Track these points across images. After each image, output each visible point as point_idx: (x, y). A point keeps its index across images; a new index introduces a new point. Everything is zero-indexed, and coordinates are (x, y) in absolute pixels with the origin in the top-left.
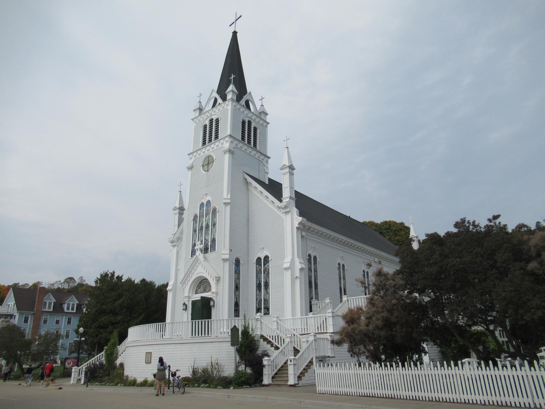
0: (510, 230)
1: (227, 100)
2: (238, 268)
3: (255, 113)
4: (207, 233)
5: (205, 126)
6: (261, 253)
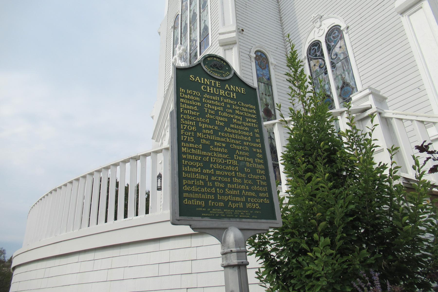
2: (264, 71)
6: (317, 30)
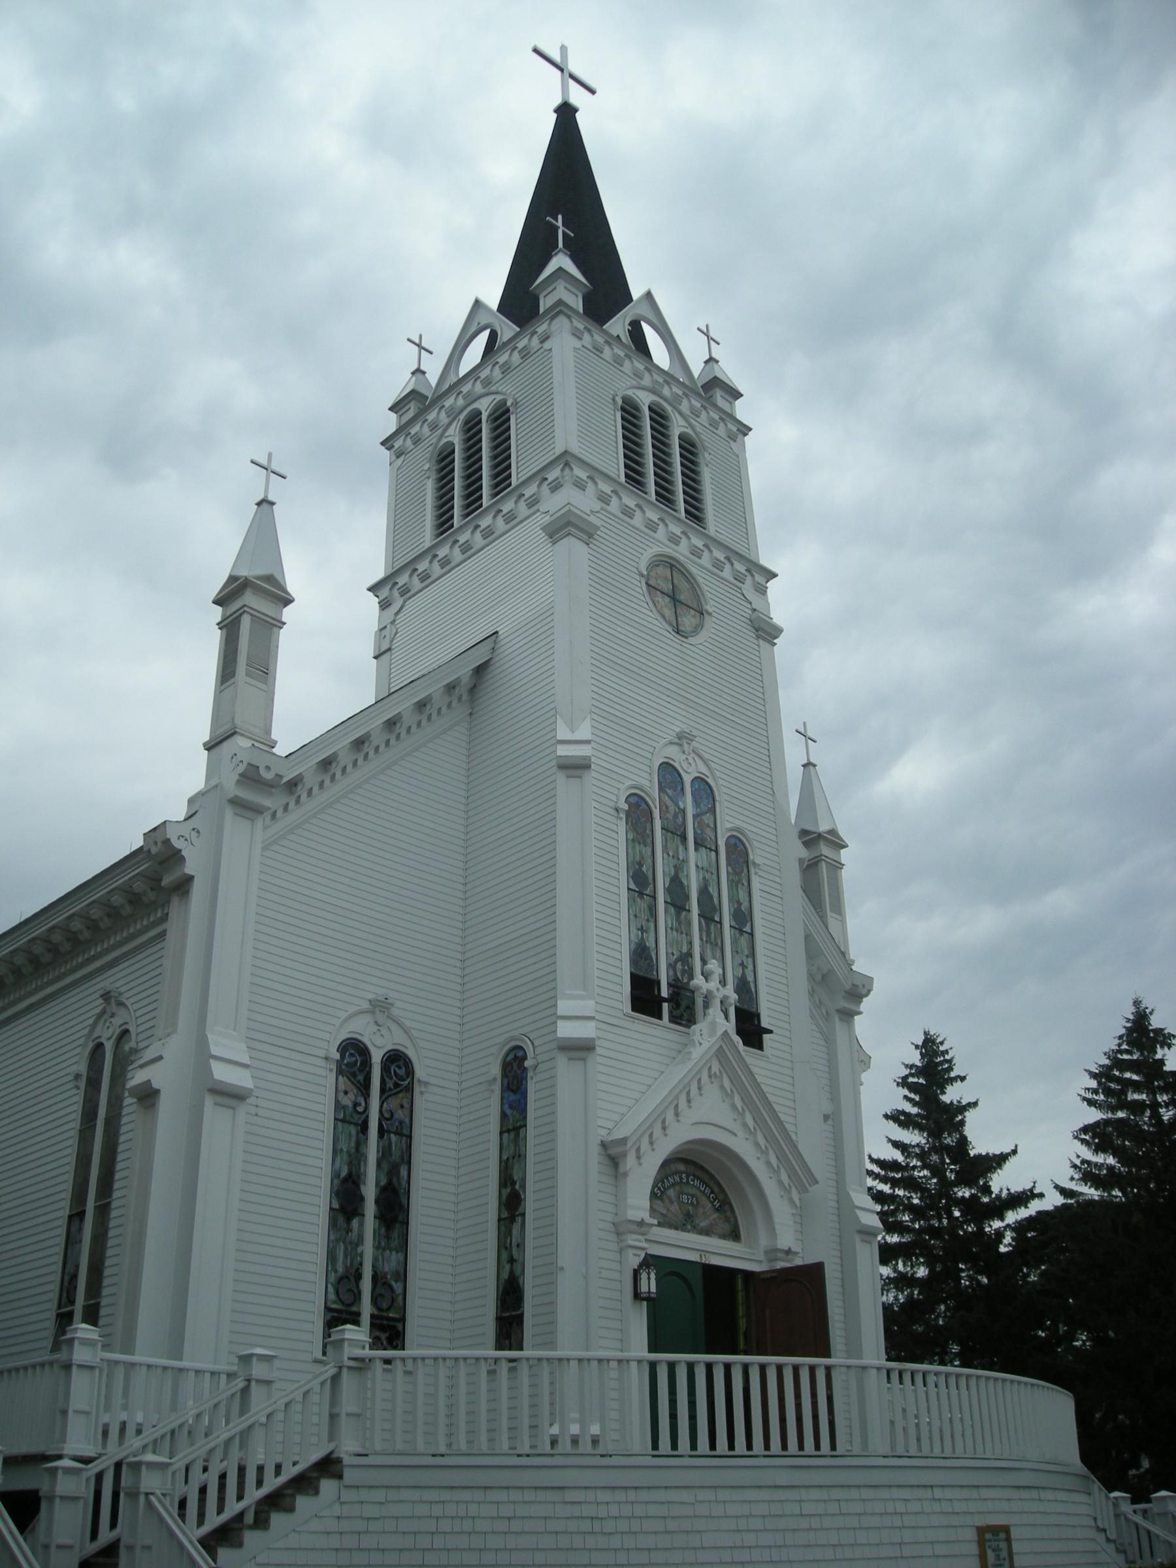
0: (1165, 1068)
1: (541, 311)
3: (681, 380)
5: (444, 459)
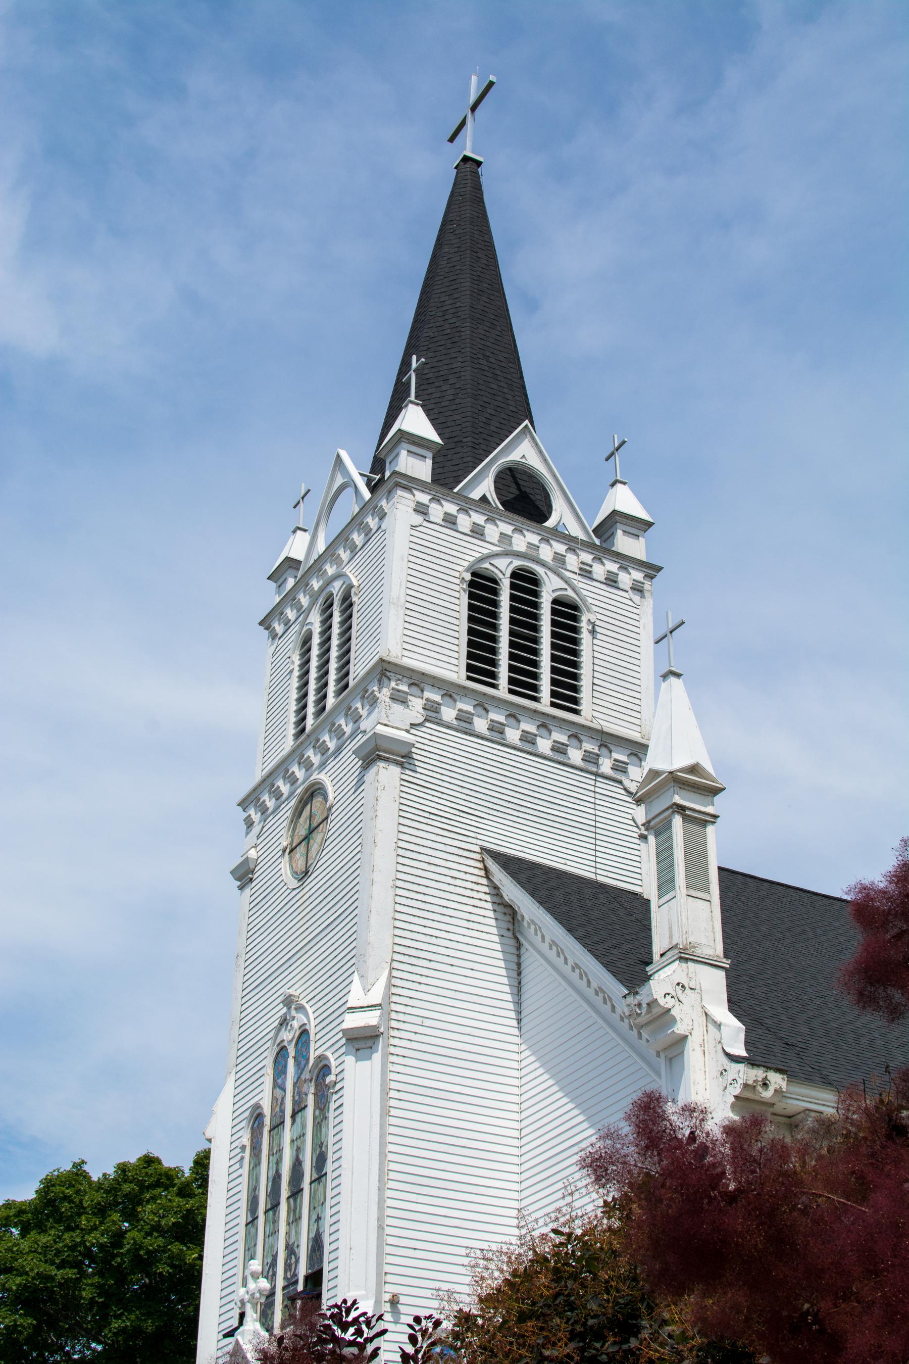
4: (294, 1219)
